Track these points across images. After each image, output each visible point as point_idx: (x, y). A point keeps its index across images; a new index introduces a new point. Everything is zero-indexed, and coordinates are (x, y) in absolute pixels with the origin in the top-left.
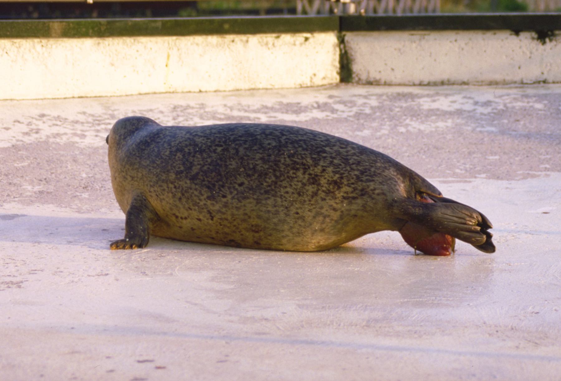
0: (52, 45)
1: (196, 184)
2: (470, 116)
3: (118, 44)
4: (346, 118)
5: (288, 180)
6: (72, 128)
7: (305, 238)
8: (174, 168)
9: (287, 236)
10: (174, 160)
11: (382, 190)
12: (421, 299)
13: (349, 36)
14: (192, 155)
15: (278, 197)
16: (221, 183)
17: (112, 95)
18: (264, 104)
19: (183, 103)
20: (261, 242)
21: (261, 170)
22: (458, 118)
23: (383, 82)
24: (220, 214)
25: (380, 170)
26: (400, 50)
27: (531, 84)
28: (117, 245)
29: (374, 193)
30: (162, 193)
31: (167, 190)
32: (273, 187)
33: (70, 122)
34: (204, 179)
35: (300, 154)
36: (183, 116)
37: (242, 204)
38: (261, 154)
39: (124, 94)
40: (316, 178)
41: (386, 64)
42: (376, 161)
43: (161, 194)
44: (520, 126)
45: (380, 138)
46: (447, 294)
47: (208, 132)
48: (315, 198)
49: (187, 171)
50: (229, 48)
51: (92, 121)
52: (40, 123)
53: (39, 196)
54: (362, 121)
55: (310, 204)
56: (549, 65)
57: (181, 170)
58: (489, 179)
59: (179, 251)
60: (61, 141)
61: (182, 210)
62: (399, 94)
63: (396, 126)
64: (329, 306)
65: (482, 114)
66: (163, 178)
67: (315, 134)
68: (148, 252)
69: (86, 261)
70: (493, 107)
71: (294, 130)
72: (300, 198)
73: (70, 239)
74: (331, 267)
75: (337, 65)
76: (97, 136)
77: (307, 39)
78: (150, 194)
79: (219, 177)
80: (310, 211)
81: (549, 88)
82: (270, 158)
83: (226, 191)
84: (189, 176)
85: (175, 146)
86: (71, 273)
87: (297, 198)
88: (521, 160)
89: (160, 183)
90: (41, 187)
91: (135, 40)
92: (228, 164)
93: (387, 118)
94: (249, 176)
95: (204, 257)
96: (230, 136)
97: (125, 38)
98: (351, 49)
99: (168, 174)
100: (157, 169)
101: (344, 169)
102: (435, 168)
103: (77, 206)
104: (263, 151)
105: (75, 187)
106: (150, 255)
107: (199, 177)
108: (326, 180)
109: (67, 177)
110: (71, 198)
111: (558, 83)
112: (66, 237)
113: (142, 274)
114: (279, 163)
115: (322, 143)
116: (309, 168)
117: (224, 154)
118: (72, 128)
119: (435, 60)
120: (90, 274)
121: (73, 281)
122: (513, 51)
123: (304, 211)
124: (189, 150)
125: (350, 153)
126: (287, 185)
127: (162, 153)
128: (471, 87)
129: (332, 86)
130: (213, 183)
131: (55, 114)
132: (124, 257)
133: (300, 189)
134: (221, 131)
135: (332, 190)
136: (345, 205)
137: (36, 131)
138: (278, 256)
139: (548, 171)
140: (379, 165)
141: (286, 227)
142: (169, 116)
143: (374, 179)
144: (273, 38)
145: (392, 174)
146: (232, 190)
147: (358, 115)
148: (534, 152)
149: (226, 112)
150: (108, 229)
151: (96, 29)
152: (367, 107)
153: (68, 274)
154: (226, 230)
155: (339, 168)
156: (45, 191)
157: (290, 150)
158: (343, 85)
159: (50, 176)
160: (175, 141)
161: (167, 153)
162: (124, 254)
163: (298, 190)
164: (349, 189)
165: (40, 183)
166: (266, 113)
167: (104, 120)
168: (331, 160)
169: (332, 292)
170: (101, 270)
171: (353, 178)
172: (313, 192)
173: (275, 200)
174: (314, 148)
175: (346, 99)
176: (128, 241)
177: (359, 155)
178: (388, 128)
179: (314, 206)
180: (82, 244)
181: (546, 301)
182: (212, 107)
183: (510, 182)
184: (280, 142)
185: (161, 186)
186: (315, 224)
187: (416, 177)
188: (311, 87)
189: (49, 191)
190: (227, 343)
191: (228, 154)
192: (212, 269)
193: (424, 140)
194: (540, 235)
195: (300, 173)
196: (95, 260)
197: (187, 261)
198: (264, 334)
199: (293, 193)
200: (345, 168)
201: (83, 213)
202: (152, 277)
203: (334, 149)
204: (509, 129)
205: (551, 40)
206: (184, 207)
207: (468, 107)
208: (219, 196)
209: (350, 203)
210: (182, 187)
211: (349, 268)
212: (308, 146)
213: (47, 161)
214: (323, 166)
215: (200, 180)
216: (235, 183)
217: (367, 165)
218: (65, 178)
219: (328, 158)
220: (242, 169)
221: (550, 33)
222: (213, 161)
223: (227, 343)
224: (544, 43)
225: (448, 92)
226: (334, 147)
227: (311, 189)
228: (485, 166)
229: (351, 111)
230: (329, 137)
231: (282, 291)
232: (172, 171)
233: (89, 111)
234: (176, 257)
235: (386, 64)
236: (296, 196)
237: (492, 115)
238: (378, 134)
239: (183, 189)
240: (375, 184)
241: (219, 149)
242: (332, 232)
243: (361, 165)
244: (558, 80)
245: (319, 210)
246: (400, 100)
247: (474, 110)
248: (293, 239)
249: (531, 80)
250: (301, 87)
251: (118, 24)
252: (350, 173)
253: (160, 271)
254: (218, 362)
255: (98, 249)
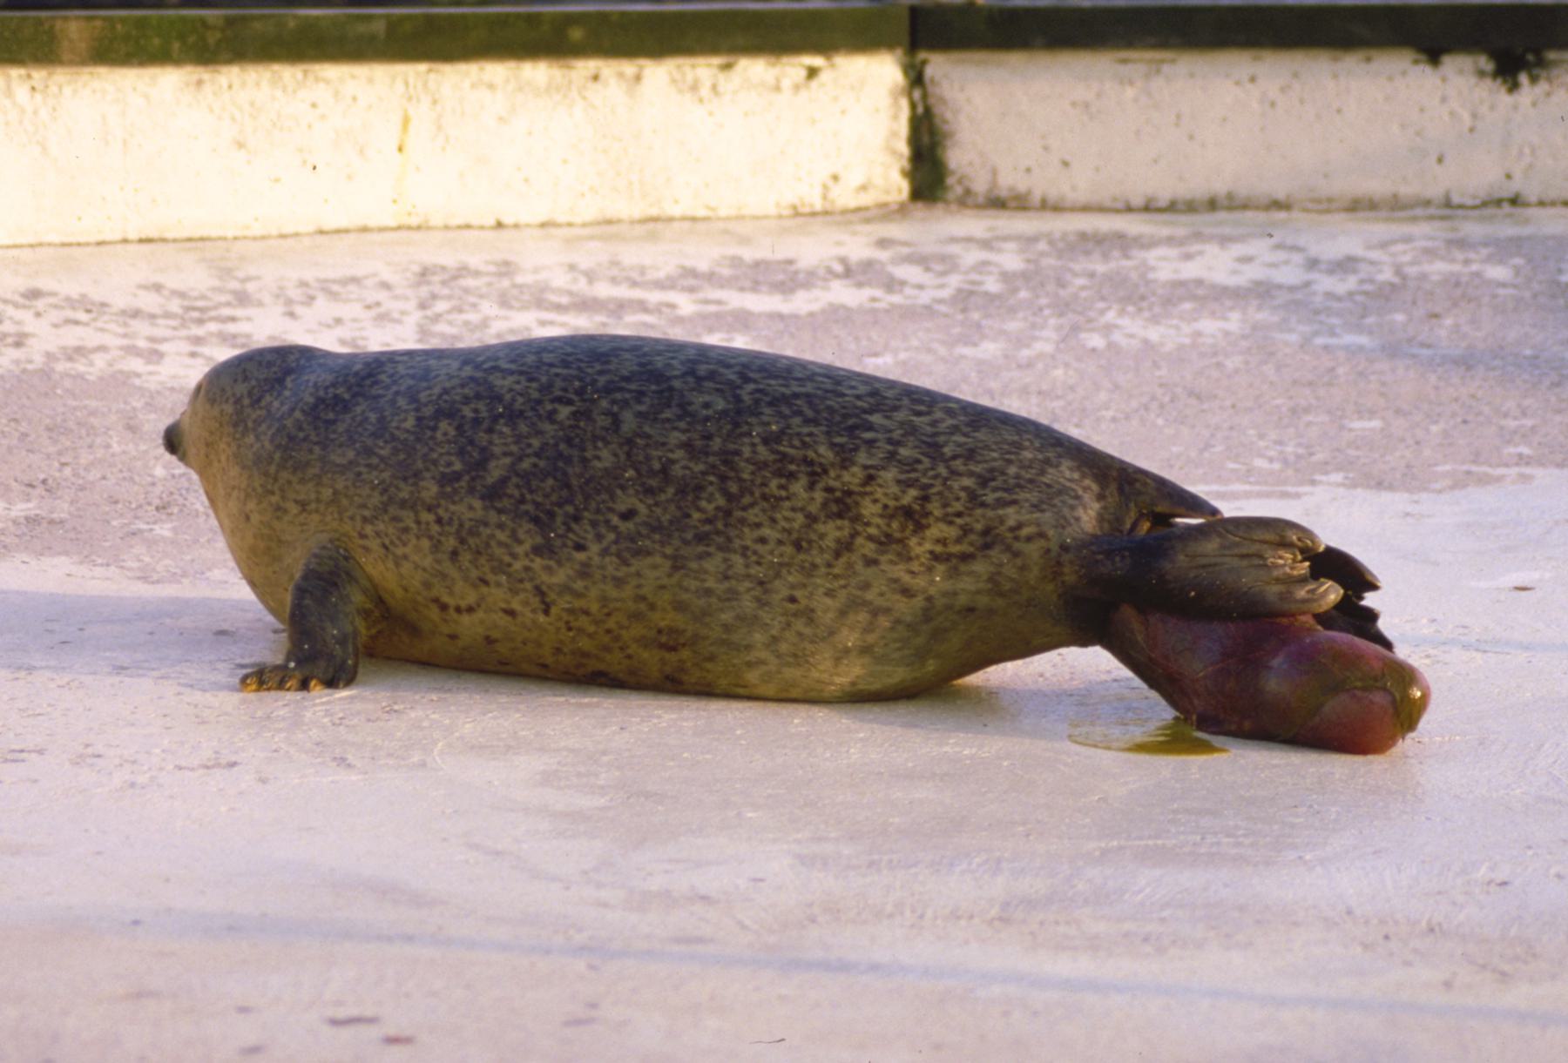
0: (60, 88)
1: (500, 511)
2: (1296, 302)
3: (258, 84)
4: (927, 307)
5: (765, 504)
6: (121, 330)
7: (813, 669)
8: (432, 468)
9: (763, 662)
10: (431, 443)
11: (1038, 525)
12: (1160, 842)
13: (938, 66)
14: (485, 425)
15: (735, 552)
16: (570, 509)
17: (239, 233)
18: (689, 263)
19: (449, 259)
20: (685, 678)
21: (684, 477)
22: (1259, 308)
23: (1036, 198)
24: (568, 598)
25: (1034, 471)
26: (1087, 105)
27: (1474, 207)
28: (262, 678)
29: (1017, 538)
30: (399, 539)
31: (415, 531)
32: (720, 525)
33: (116, 314)
34: (522, 495)
35: (798, 434)
36: (449, 298)
37: (632, 569)
38: (684, 431)
39: (274, 232)
40: (849, 501)
41: (1046, 148)
42: (1018, 446)
43: (397, 542)
44: (1443, 333)
45: (1029, 365)
46: (1237, 827)
47: (531, 359)
48: (843, 560)
49: (473, 473)
50: (584, 98)
51: (180, 311)
52: (26, 316)
53: (25, 530)
54: (976, 316)
55: (829, 574)
56: (1527, 150)
57: (455, 472)
58: (1354, 486)
59: (444, 696)
60: (91, 370)
61: (460, 585)
62: (1083, 236)
63: (1075, 329)
64: (891, 861)
65: (1330, 295)
66: (404, 495)
67: (840, 378)
68: (352, 698)
69: (168, 725)
70: (1363, 275)
71: (779, 365)
72: (802, 556)
73: (123, 658)
74: (891, 745)
75: (904, 148)
76: (193, 355)
77: (812, 72)
78: (361, 542)
79: (565, 493)
80: (830, 593)
81: (1527, 221)
82: (711, 443)
83: (586, 531)
84: (479, 488)
85: (430, 402)
86: (126, 761)
87: (792, 558)
88: (1445, 434)
89: (393, 510)
90: (30, 505)
91: (305, 72)
92: (588, 454)
93: (1048, 306)
94: (649, 491)
95: (518, 715)
96: (596, 377)
97: (276, 67)
98: (943, 101)
99: (415, 484)
100: (382, 471)
101: (931, 473)
102: (1193, 454)
103: (139, 561)
104: (689, 423)
105: (134, 506)
106: (358, 706)
107: (509, 491)
108: (879, 506)
109: (109, 475)
110: (122, 538)
111: (1553, 204)
112: (108, 654)
113: (335, 764)
114: (737, 458)
115: (859, 403)
116: (825, 471)
117: (577, 427)
118: (121, 330)
119: (1191, 137)
120: (184, 764)
121: (133, 785)
122: (1422, 110)
123: (812, 594)
124: (476, 411)
125: (942, 427)
126: (762, 518)
127: (394, 424)
128: (1296, 214)
129: (886, 213)
130: (548, 507)
131: (71, 288)
132: (281, 713)
133: (799, 531)
134: (570, 359)
135: (897, 535)
136: (938, 579)
137: (16, 339)
138: (737, 713)
139: (1528, 464)
140: (1027, 455)
141: (758, 637)
142: (406, 298)
143: (1015, 497)
144: (715, 71)
145: (1065, 478)
146: (603, 530)
147: (964, 298)
148: (1486, 410)
149: (574, 288)
150: (234, 629)
151: (191, 39)
152: (990, 273)
153: (117, 761)
154: (584, 644)
155: (915, 470)
156: (43, 518)
157: (768, 424)
158: (920, 210)
159: (57, 474)
160: (429, 388)
161: (410, 423)
162: (283, 703)
163: (795, 536)
164: (952, 532)
165: (28, 495)
166: (692, 290)
167: (216, 308)
168: (890, 448)
169: (897, 820)
170: (216, 752)
171: (958, 499)
172: (838, 541)
173: (726, 560)
174: (837, 418)
175: (930, 248)
176: (294, 669)
177: (969, 429)
178: (1054, 336)
179: (842, 582)
180: (155, 674)
181: (1530, 847)
182: (536, 270)
183: (1415, 497)
184: (738, 399)
185: (395, 519)
186: (845, 631)
187: (1139, 476)
188: (826, 213)
189: (55, 516)
190: (591, 967)
191: (590, 428)
192: (542, 750)
193: (1158, 373)
194: (1508, 654)
195: (798, 487)
196: (197, 720)
197: (467, 726)
198: (700, 940)
199: (780, 542)
200: (932, 469)
201: (158, 582)
202: (366, 773)
203: (898, 419)
204: (1410, 340)
205: (1534, 80)
206: (466, 579)
207: (1289, 275)
208: (564, 545)
209: (954, 573)
210: (459, 519)
211: (946, 749)
212: (817, 412)
213: (49, 429)
214: (866, 467)
215: (513, 501)
216: (611, 510)
217: (994, 460)
218: (104, 478)
219: (878, 444)
220: (630, 473)
221: (1530, 57)
222: (547, 444)
223: (591, 967)
224: (1514, 87)
225: (1227, 230)
226: (895, 414)
227: (832, 531)
228: (1338, 450)
229: (942, 286)
230: (877, 385)
231: (750, 815)
232: (427, 475)
233: (172, 281)
234: (434, 713)
235: (1046, 148)
236: (789, 550)
237: (1359, 298)
238: (1025, 353)
239: (461, 525)
240: (1018, 512)
241: (564, 412)
242: (896, 655)
243: (979, 458)
244: (1553, 194)
245: (855, 592)
246: (1087, 253)
247: (1307, 284)
248: (779, 673)
249: (1474, 197)
250: (796, 213)
251: (257, 25)
252: (948, 483)
253: (390, 755)
254: (568, 1024)
255: (205, 691)
